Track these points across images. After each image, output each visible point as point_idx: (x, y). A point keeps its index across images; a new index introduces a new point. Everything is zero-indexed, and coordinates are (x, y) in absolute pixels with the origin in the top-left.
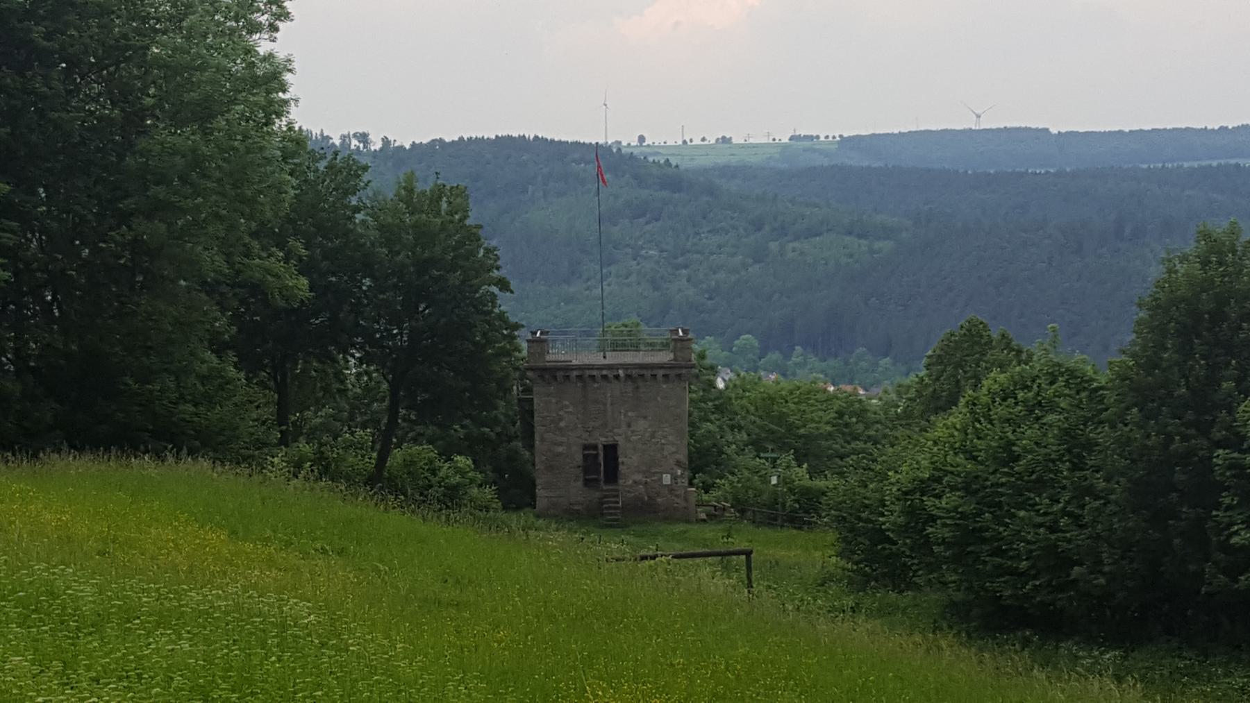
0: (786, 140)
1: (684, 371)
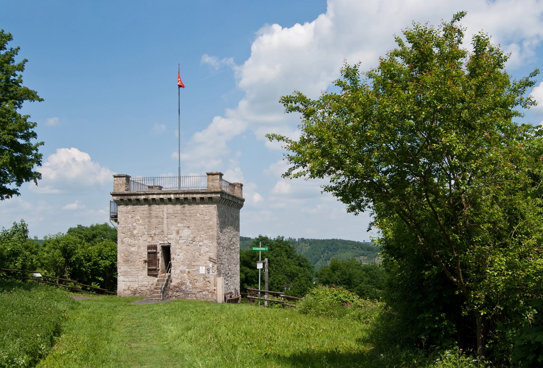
1: (213, 195)
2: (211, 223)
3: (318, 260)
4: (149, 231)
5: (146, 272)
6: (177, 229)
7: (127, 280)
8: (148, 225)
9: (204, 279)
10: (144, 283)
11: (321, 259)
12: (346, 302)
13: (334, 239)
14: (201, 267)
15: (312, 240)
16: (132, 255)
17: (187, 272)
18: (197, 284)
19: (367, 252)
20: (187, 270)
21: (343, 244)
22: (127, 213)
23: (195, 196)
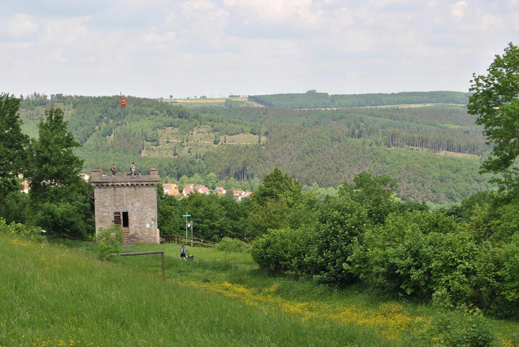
0: (227, 97)
1: (154, 183)
3: (88, 136)
9: (149, 231)
11: (94, 134)
12: (240, 245)
15: (77, 97)
16: (104, 218)
18: (145, 234)
19: (178, 119)
20: (139, 226)
21: (134, 105)
22: (100, 193)
23: (143, 183)
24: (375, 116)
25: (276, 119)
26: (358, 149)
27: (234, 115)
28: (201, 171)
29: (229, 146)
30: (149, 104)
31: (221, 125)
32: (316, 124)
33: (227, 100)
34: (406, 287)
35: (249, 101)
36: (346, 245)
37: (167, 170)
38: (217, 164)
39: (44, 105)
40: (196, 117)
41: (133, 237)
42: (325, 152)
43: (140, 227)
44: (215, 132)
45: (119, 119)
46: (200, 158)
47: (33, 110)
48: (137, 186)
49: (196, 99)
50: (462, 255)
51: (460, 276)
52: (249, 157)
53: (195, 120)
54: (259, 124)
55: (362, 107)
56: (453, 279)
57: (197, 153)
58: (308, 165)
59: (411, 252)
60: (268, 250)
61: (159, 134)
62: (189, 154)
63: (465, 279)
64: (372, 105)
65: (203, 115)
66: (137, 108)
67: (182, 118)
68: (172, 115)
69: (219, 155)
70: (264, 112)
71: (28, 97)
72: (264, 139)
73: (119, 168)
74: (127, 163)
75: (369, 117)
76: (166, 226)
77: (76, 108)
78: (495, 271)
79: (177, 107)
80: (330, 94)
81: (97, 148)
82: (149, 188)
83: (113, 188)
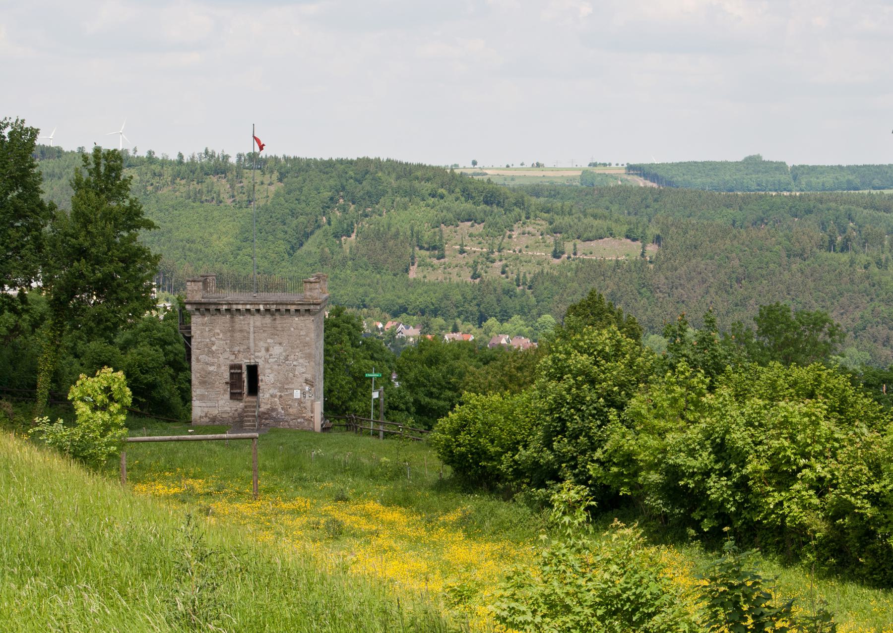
0: (585, 165)
1: (312, 307)
2: (308, 339)
3: (307, 236)
4: (231, 347)
5: (228, 396)
6: (266, 345)
7: (204, 405)
8: (230, 340)
9: (299, 404)
10: (226, 408)
11: (318, 232)
13: (367, 161)
14: (295, 391)
15: (287, 159)
16: (210, 376)
17: (278, 396)
18: (291, 410)
19: (483, 206)
20: (279, 394)
22: (203, 325)
23: (289, 307)
24: (878, 210)
25: (679, 211)
26: (840, 273)
27: (597, 201)
28: (526, 310)
29: (583, 261)
30: (427, 176)
31: (567, 219)
32: (759, 222)
33: (585, 172)
34: (703, 517)
35: (629, 174)
36: (600, 427)
37: (457, 307)
38: (557, 297)
39: (222, 173)
40: (520, 203)
41: (267, 416)
42: (774, 279)
43: (281, 397)
44: (555, 233)
45: (368, 203)
46: (524, 284)
47: (202, 182)
48: (277, 314)
49: (523, 169)
50: (810, 448)
51: (804, 493)
52: (621, 284)
53: (517, 210)
54: (645, 219)
55: (852, 192)
56: (790, 499)
57: (518, 275)
58: (740, 304)
59: (714, 441)
60: (463, 437)
61: (445, 236)
62: (504, 276)
63: (812, 501)
64: (874, 188)
65: (534, 200)
66: (404, 183)
67: (492, 204)
68: (472, 198)
69: (562, 280)
70: (655, 196)
71: (193, 157)
72: (652, 249)
73: (363, 301)
74: (380, 290)
75: (865, 211)
76: (360, 401)
77: (286, 180)
78: (869, 482)
79: (483, 182)
80: (790, 164)
81: (323, 261)
82: (302, 318)
83: (228, 316)
